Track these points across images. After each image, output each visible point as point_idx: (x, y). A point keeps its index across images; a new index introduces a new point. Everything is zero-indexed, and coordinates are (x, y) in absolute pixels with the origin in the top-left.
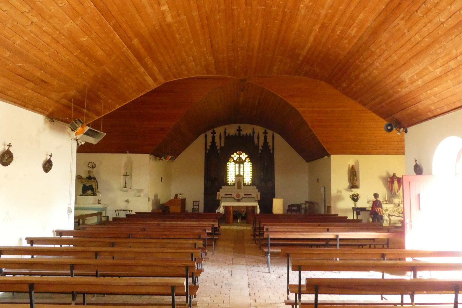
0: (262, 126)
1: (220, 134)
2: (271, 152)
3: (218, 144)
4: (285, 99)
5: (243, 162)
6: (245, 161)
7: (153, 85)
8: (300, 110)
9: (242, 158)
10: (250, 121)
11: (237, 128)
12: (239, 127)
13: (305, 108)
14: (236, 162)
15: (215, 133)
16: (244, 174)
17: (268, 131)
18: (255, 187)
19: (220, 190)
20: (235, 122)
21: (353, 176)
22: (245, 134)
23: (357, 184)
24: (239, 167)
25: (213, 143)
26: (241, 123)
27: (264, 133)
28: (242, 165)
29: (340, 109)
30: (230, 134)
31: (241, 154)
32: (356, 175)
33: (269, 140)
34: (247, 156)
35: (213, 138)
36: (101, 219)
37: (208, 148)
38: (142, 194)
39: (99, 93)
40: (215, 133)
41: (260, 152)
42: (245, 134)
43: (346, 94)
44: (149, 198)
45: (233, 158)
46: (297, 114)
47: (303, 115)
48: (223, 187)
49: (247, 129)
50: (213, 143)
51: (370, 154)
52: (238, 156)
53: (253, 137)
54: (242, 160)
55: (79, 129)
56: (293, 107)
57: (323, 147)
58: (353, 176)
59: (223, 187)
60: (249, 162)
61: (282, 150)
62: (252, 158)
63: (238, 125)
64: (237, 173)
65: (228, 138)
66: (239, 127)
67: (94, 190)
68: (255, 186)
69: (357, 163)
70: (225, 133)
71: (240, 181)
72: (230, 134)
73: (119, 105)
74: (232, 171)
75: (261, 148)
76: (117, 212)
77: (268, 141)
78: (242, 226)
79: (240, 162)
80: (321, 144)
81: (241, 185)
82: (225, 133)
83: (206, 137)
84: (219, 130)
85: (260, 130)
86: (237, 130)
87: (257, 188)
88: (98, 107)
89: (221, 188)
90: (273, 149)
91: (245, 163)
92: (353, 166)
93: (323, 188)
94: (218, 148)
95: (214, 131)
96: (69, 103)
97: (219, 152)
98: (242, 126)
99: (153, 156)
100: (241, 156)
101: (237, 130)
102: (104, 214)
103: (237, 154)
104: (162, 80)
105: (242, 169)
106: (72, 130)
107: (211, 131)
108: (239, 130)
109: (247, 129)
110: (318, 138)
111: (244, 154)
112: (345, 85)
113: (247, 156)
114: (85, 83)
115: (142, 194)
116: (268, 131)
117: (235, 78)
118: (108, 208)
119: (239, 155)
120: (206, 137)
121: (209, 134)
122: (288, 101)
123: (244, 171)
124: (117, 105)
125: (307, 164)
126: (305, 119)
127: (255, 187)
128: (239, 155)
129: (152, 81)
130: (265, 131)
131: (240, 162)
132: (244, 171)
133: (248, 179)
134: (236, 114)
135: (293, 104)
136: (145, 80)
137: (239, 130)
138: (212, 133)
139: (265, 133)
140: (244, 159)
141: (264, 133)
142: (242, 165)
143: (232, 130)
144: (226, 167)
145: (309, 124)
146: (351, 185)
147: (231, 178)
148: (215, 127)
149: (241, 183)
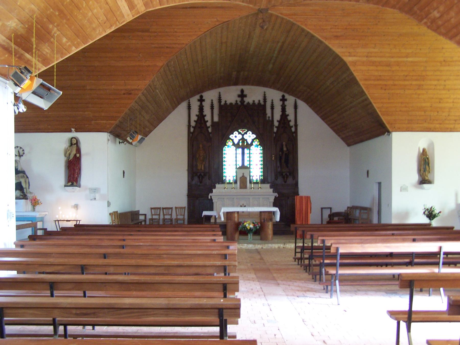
0: (278, 89)
1: (212, 102)
2: (293, 129)
3: (208, 118)
4: (327, 43)
5: (249, 146)
6: (252, 144)
7: (128, 16)
8: (348, 59)
9: (246, 140)
10: (260, 82)
11: (239, 93)
12: (242, 91)
13: (357, 59)
14: (237, 146)
15: (204, 100)
16: (250, 165)
17: (287, 96)
18: (268, 186)
19: (214, 190)
20: (236, 84)
21: (425, 164)
22: (251, 102)
23: (429, 177)
24: (243, 154)
25: (201, 116)
26: (244, 84)
27: (281, 100)
28: (246, 151)
29: (410, 59)
30: (228, 102)
31: (246, 133)
32: (429, 164)
33: (290, 111)
34: (255, 136)
35: (201, 109)
36: (36, 232)
37: (193, 124)
38: (97, 196)
39: (51, 26)
40: (204, 100)
41: (275, 130)
42: (251, 102)
43: (437, 30)
44: (108, 202)
45: (233, 140)
46: (344, 67)
47: (352, 68)
48: (217, 186)
49: (254, 94)
50: (201, 116)
51: (451, 130)
52: (240, 137)
53: (264, 106)
54: (247, 142)
55: (27, 82)
56: (337, 56)
57: (381, 120)
58: (425, 164)
59: (217, 186)
60: (257, 146)
61: (310, 127)
62: (262, 139)
63: (240, 87)
64: (240, 164)
65: (225, 109)
66: (242, 91)
67: (25, 190)
68: (268, 183)
69: (432, 145)
70: (220, 100)
71: (245, 175)
72: (228, 102)
73: (77, 48)
74: (231, 158)
75: (276, 124)
76: (57, 222)
77: (287, 113)
78: (254, 244)
79: (244, 146)
80: (378, 116)
81: (246, 182)
82: (220, 100)
83: (189, 107)
84: (210, 96)
85: (274, 95)
86: (239, 96)
87: (271, 187)
88: (46, 50)
89: (215, 188)
90: (296, 125)
91: (252, 148)
92: (424, 150)
93: (376, 187)
94: (209, 124)
95: (201, 97)
96: (8, 41)
97: (210, 130)
98: (248, 89)
99: (112, 136)
100: (246, 137)
101: (239, 96)
102: (39, 225)
103: (240, 133)
104: (142, 9)
105: (246, 156)
106: (16, 85)
107: (198, 97)
108: (242, 95)
109: (254, 94)
110: (374, 105)
111: (250, 133)
112: (436, 14)
113: (255, 136)
114: (33, 6)
115: (97, 196)
116: (287, 96)
117: (251, 6)
118: (46, 219)
119: (243, 135)
120: (189, 107)
121: (195, 102)
122: (330, 46)
123: (250, 161)
124: (74, 48)
125: (348, 148)
126: (355, 74)
127: (268, 186)
128: (243, 135)
129: (127, 8)
130: (283, 96)
131: (244, 146)
132: (250, 161)
133: (256, 173)
134: (240, 70)
135: (338, 50)
136: (118, 8)
137: (242, 95)
138: (199, 100)
139: (283, 99)
140: (249, 142)
141: (281, 100)
142: (246, 151)
143: (230, 95)
144: (222, 154)
145: (361, 83)
146: (421, 179)
147: (230, 172)
148: (203, 91)
149: (246, 178)
